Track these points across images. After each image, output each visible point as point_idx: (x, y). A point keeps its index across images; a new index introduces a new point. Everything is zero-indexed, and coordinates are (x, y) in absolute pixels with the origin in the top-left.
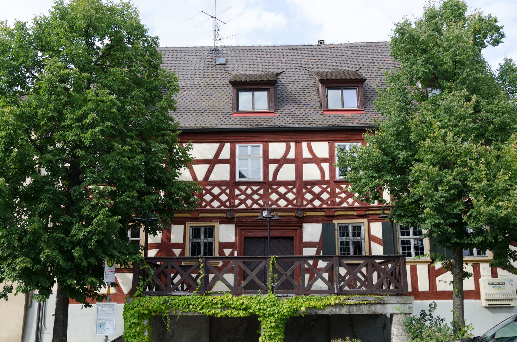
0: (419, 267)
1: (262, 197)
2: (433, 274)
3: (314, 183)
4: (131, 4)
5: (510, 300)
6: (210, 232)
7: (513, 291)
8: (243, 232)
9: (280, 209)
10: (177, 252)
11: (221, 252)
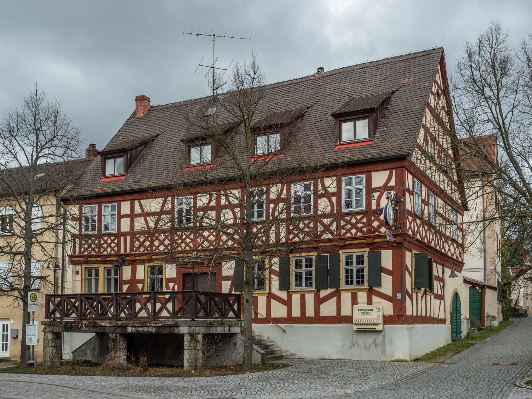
0: (307, 295)
1: (192, 240)
2: (319, 301)
3: (228, 227)
4: (59, 100)
5: (375, 324)
6: (161, 271)
7: (379, 316)
8: (182, 269)
9: (204, 250)
10: (140, 286)
11: (167, 287)
